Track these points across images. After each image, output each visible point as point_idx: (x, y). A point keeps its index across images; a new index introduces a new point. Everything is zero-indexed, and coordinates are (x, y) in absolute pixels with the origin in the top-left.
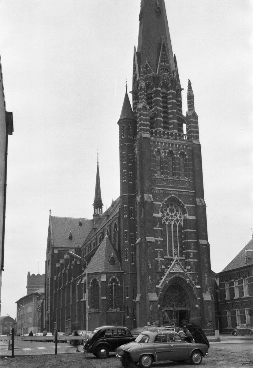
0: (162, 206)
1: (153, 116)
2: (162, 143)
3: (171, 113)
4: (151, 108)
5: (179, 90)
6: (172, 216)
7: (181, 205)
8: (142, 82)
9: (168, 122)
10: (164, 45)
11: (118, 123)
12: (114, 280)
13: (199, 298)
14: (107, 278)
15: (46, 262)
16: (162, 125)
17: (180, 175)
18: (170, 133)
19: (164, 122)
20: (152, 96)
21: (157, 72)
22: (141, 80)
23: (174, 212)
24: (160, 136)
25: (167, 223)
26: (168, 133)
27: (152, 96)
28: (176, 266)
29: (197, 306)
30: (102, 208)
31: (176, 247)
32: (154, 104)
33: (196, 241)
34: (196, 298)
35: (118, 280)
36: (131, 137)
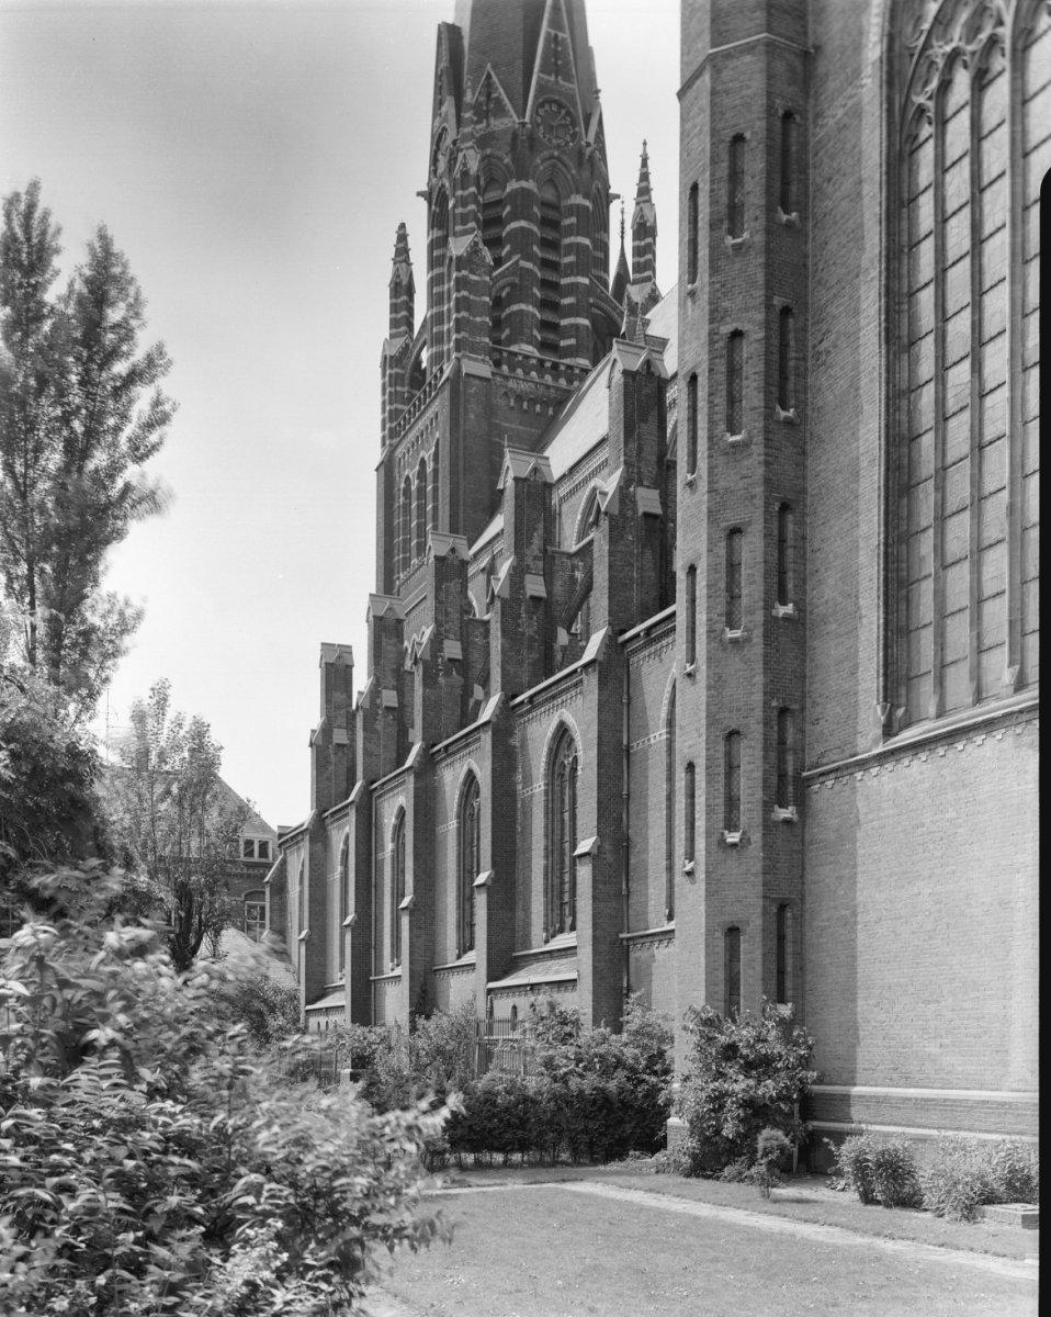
1: (504, 294)
3: (571, 248)
4: (498, 262)
5: (604, 198)
8: (467, 149)
9: (558, 223)
18: (562, 368)
19: (543, 238)
20: (504, 234)
22: (465, 138)
24: (527, 373)
26: (555, 366)
27: (504, 234)
32: (508, 248)
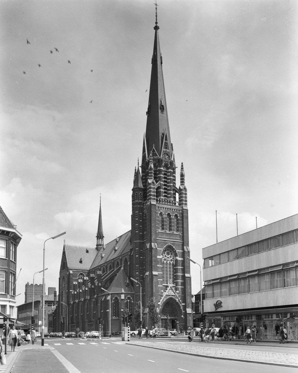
0: (162, 251)
2: (163, 208)
6: (168, 258)
7: (174, 250)
10: (166, 135)
11: (132, 190)
12: (129, 298)
13: (184, 311)
14: (125, 297)
15: (59, 279)
16: (163, 195)
17: (174, 230)
21: (161, 156)
23: (169, 255)
25: (165, 262)
29: (182, 316)
30: (103, 239)
31: (170, 278)
33: (183, 274)
34: (182, 311)
35: (131, 298)
36: (142, 201)
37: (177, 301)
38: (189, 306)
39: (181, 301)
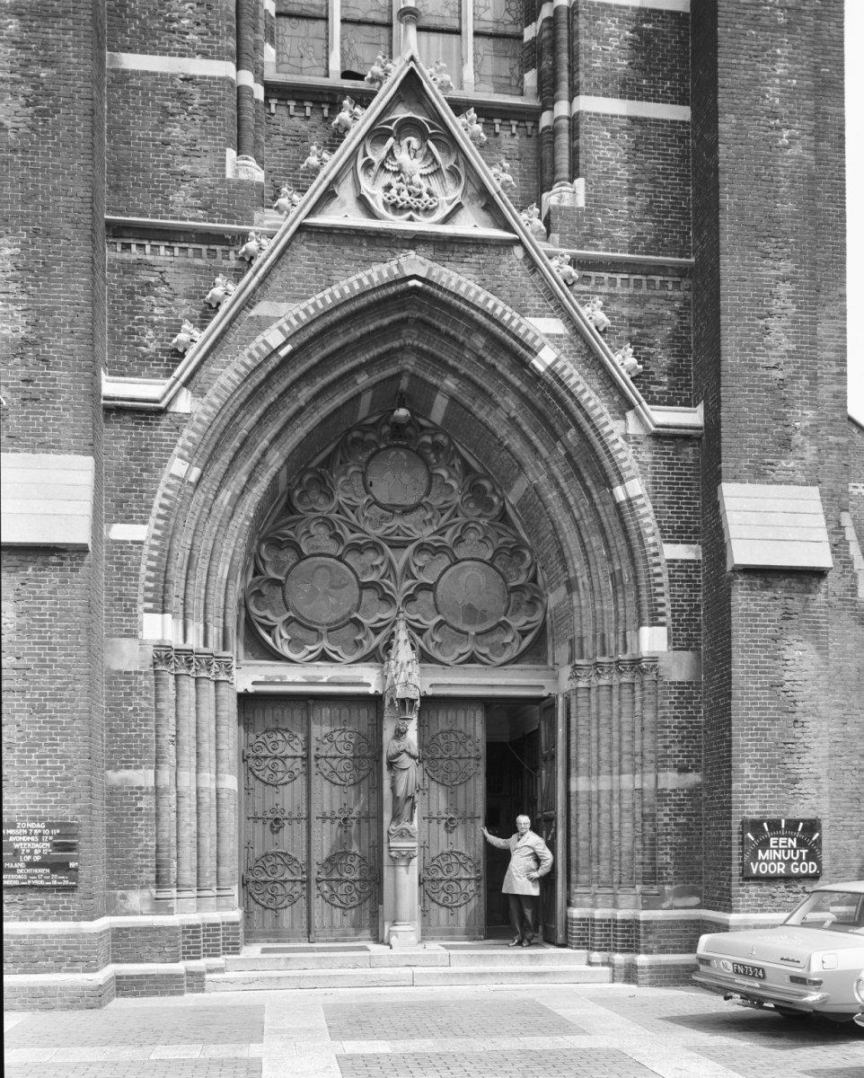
28: (403, 157)
29: (652, 640)
37: (545, 358)
38: (785, 444)
39: (623, 361)
